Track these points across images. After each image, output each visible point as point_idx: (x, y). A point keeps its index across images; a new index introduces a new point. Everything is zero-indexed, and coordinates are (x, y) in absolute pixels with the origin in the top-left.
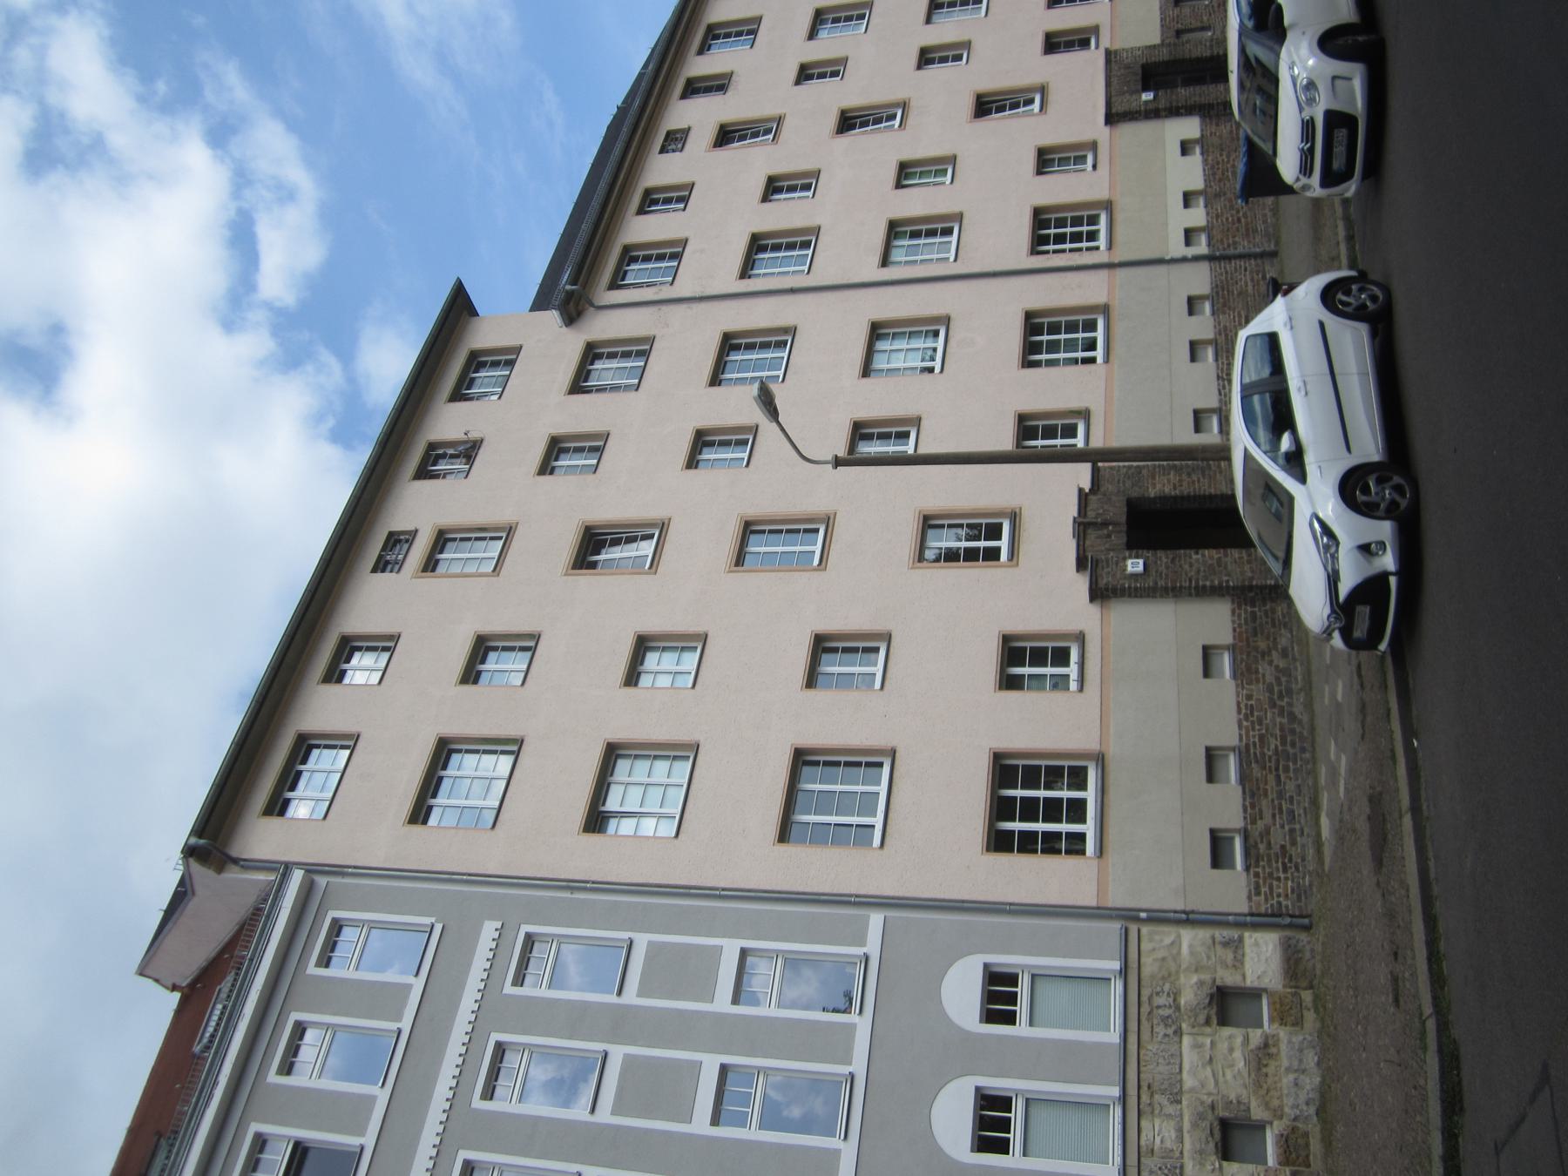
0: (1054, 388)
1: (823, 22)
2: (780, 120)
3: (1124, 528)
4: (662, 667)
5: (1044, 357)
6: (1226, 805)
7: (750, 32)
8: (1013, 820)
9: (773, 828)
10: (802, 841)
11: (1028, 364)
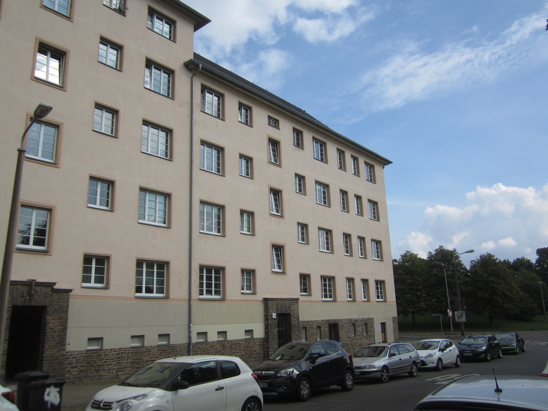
0: (122, 275)
1: (324, 188)
2: (280, 166)
3: (27, 304)
4: (160, 138)
5: (205, 274)
7: (371, 180)
8: (96, 265)
9: (205, 198)
10: (90, 185)
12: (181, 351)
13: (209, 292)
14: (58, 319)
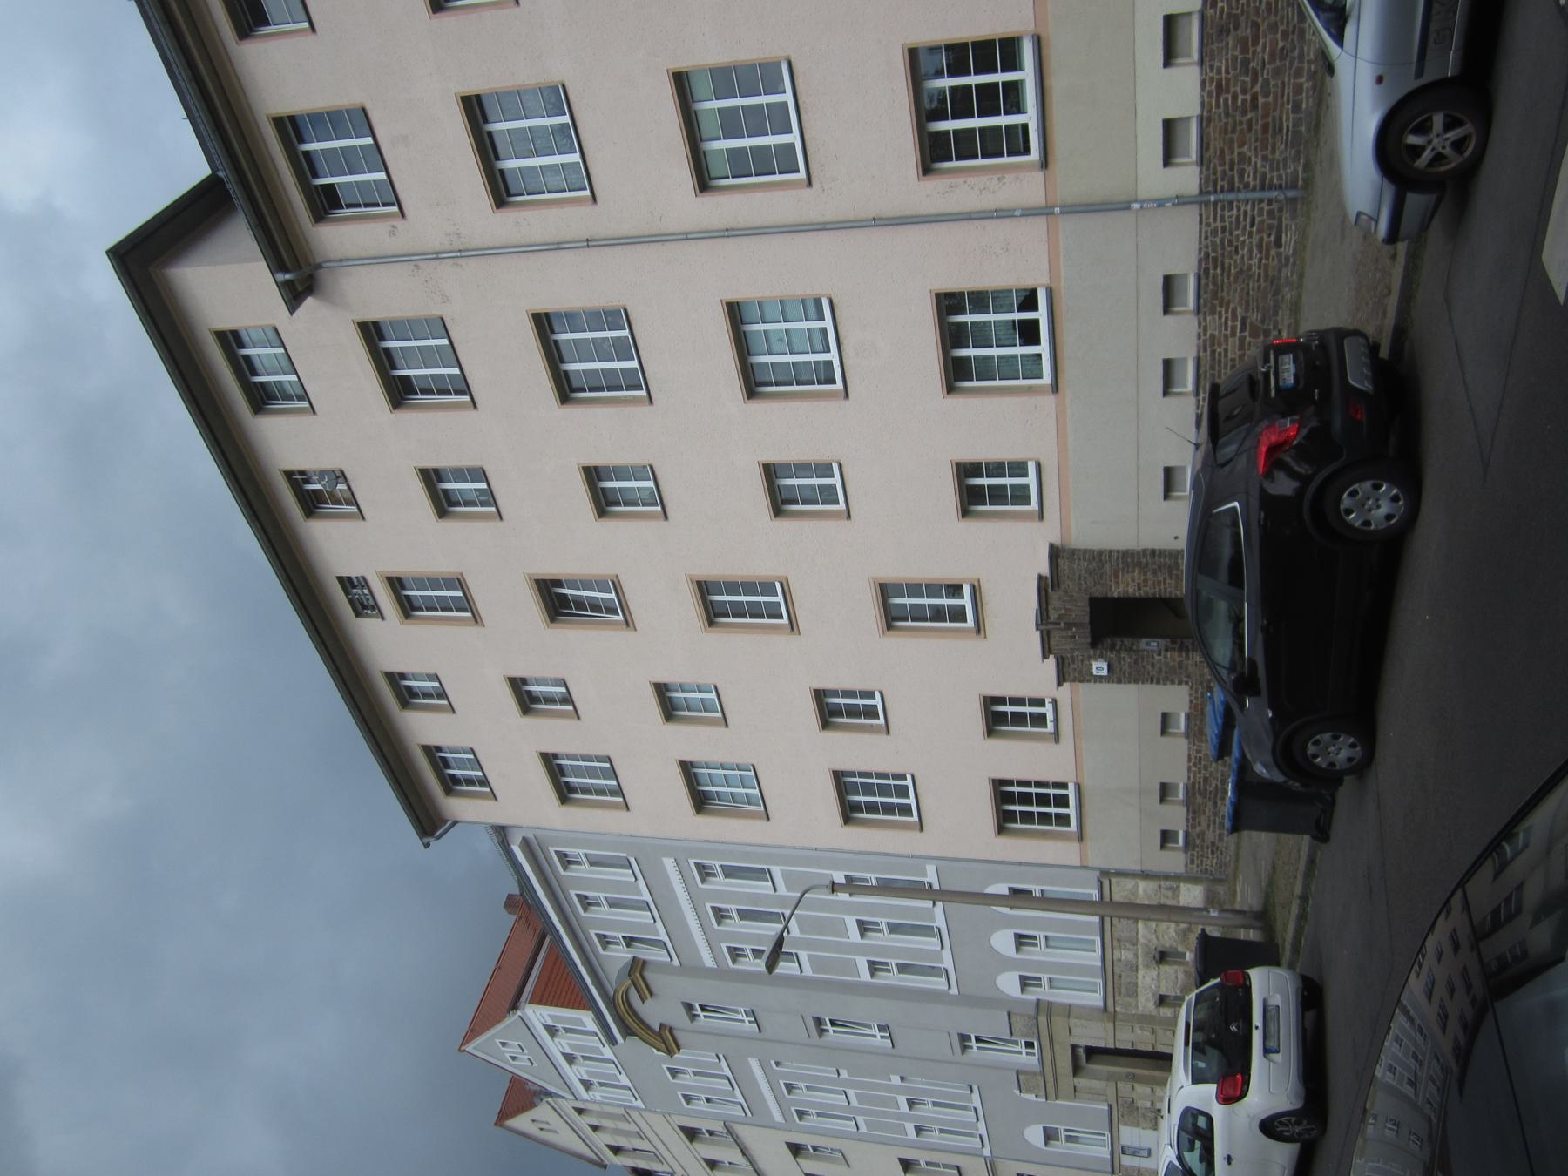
0: (996, 424)
6: (1175, 817)
11: (950, 389)
12: (1224, 229)
13: (1012, 97)
14: (1117, 576)
